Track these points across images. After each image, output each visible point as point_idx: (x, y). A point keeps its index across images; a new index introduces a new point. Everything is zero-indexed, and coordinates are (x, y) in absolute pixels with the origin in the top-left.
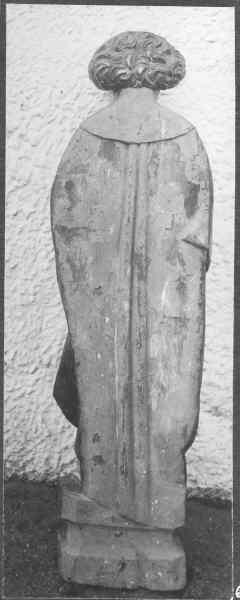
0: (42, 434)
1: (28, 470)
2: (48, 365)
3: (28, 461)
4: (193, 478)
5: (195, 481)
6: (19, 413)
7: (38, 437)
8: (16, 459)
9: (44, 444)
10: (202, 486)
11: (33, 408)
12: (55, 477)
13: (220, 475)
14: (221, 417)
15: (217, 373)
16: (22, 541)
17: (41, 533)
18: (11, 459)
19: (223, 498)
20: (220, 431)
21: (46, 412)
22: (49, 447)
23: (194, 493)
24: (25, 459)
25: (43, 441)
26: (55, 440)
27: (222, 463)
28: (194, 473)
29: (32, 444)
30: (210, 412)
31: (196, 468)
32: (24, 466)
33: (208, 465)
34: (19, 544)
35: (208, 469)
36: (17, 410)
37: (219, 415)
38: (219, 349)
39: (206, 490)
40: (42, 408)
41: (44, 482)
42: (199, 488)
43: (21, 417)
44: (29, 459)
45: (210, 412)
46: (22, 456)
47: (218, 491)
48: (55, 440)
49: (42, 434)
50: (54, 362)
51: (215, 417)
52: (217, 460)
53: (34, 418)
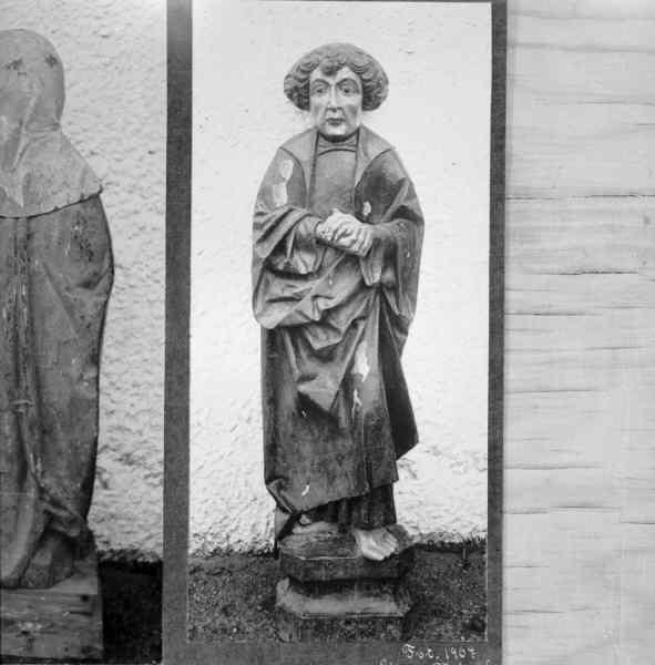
0: (246, 498)
1: (232, 541)
2: (249, 420)
3: (232, 531)
4: (104, 539)
5: (107, 543)
6: (218, 478)
7: (241, 503)
8: (218, 530)
9: (248, 510)
10: (423, 532)
11: (234, 470)
12: (264, 544)
13: (135, 533)
14: (134, 466)
15: (128, 415)
16: (228, 626)
17: (250, 613)
18: (211, 531)
19: (447, 541)
20: (134, 481)
21: (248, 473)
22: (255, 511)
23: (108, 556)
24: (228, 530)
25: (247, 507)
26: (261, 504)
27: (442, 505)
28: (106, 533)
29: (236, 512)
30: (121, 460)
31: (109, 528)
32: (228, 537)
33: (123, 522)
34: (224, 631)
35: (123, 526)
36: (216, 474)
37: (131, 464)
38: (128, 386)
39: (121, 551)
40: (244, 470)
41: (251, 552)
42: (111, 551)
43: (221, 482)
44: (233, 528)
45: (121, 460)
46: (226, 526)
47: (134, 552)
48: (261, 504)
49: (246, 498)
50: (255, 414)
51: (127, 467)
52: (130, 515)
53: (236, 481)
